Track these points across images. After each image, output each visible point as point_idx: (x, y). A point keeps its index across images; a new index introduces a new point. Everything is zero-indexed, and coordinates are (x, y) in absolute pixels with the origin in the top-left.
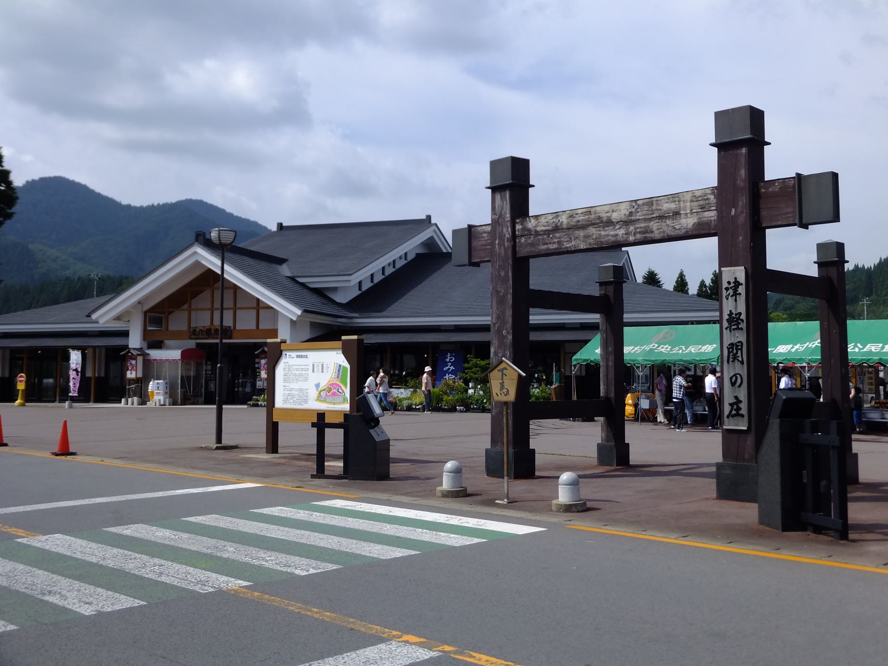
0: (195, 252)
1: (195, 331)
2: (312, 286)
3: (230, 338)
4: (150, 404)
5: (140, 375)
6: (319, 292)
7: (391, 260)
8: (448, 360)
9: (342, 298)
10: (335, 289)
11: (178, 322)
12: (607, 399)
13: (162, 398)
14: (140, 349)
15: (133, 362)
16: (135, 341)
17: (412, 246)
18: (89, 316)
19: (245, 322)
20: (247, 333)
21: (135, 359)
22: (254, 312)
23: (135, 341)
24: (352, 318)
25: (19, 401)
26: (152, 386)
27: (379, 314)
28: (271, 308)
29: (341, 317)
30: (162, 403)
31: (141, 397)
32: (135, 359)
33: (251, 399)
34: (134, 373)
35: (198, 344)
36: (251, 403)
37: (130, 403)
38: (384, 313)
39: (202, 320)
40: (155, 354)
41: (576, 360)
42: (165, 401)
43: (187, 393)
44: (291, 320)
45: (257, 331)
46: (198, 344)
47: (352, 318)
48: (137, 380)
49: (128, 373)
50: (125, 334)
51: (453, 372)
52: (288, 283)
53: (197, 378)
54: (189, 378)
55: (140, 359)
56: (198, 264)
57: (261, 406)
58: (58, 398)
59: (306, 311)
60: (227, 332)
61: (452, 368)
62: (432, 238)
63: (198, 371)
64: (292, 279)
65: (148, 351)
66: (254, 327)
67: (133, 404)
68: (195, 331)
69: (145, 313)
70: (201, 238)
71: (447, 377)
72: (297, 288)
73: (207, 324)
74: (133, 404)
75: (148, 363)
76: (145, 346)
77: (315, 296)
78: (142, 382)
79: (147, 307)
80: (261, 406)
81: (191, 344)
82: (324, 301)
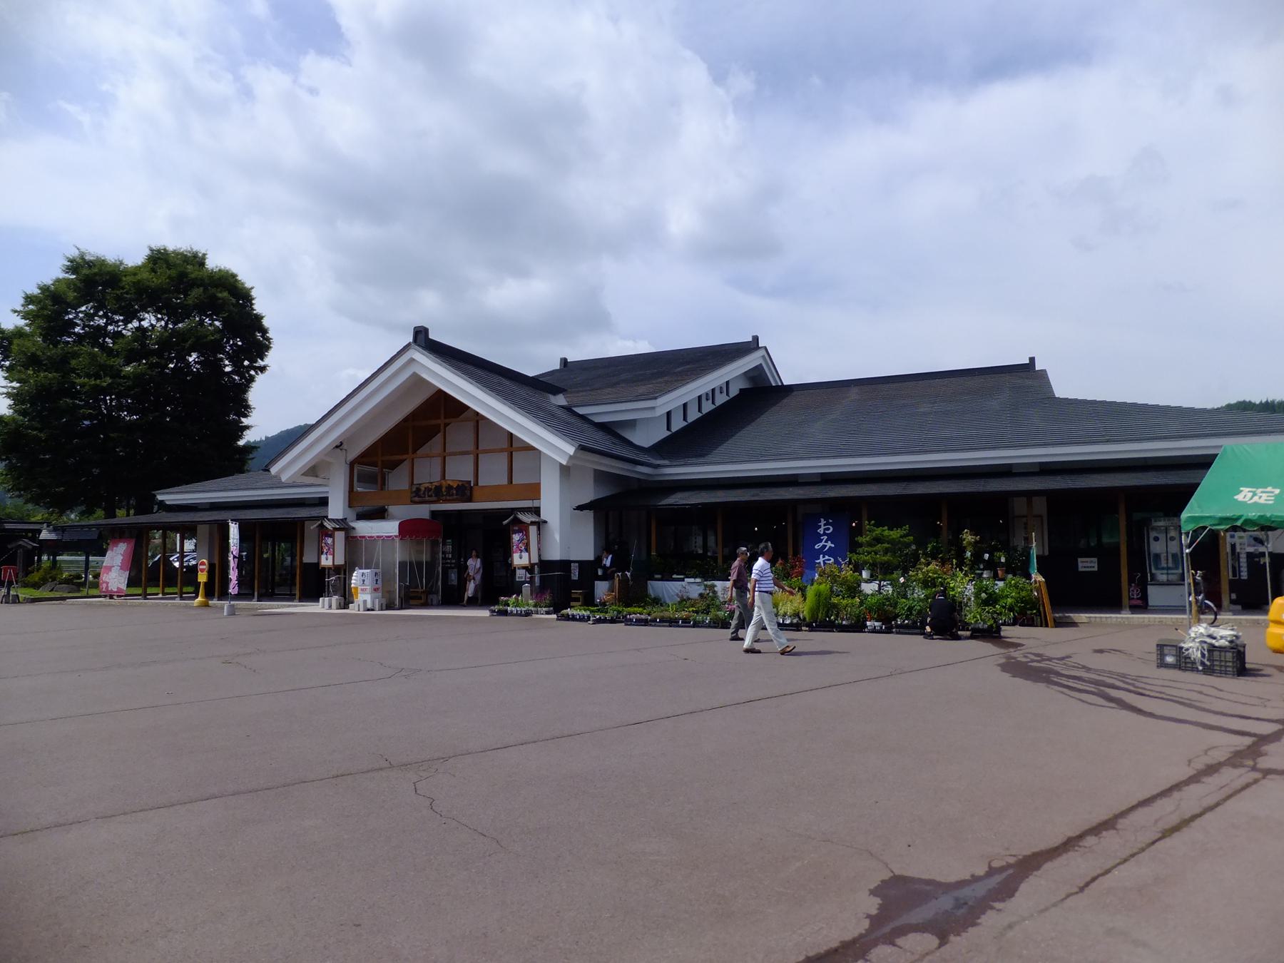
0: (412, 360)
1: (418, 490)
2: (597, 420)
3: (470, 500)
4: (353, 609)
5: (340, 561)
6: (606, 428)
7: (708, 388)
8: (821, 531)
9: (646, 437)
10: (631, 424)
11: (398, 481)
12: (609, 553)
13: (368, 597)
14: (344, 520)
15: (330, 541)
16: (337, 509)
17: (734, 371)
18: (267, 470)
19: (493, 473)
20: (495, 493)
21: (332, 536)
22: (505, 456)
23: (337, 509)
24: (658, 466)
25: (200, 599)
26: (356, 578)
27: (701, 460)
28: (533, 449)
29: (642, 464)
30: (369, 606)
31: (344, 596)
32: (332, 536)
33: (496, 602)
34: (330, 557)
35: (433, 513)
36: (496, 608)
37: (325, 606)
38: (709, 458)
39: (427, 473)
40: (365, 528)
41: (1192, 519)
42: (373, 603)
43: (420, 587)
44: (561, 465)
45: (511, 489)
46: (433, 513)
47: (658, 466)
48: (337, 569)
49: (516, 556)
50: (324, 502)
51: (831, 552)
52: (560, 413)
53: (431, 565)
54: (419, 564)
55: (340, 536)
56: (417, 382)
57: (511, 614)
58: (297, 592)
59: (582, 448)
60: (465, 491)
61: (829, 544)
62: (759, 367)
63: (434, 554)
64: (568, 409)
65: (353, 524)
66: (505, 482)
67: (330, 607)
68: (418, 490)
69: (352, 465)
70: (421, 337)
71: (821, 560)
72: (573, 420)
73: (436, 478)
74: (330, 607)
75: (352, 541)
76: (351, 515)
77: (601, 433)
78: (344, 571)
79: (354, 453)
80: (511, 614)
81: (422, 511)
82: (615, 440)
